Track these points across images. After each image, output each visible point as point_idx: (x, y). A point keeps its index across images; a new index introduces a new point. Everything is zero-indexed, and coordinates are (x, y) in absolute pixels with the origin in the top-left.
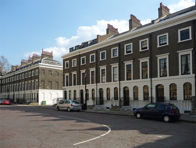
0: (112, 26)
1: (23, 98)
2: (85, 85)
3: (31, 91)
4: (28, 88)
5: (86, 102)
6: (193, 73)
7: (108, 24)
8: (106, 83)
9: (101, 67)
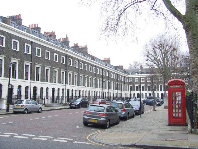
2: (8, 79)
9: (14, 58)
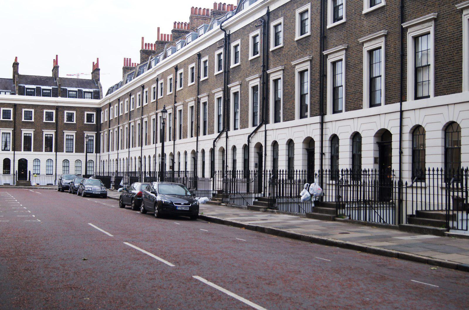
0: (130, 59)
1: (189, 169)
3: (396, 106)
4: (198, 127)
5: (185, 189)
6: (12, 151)
7: (125, 58)
8: (434, 100)
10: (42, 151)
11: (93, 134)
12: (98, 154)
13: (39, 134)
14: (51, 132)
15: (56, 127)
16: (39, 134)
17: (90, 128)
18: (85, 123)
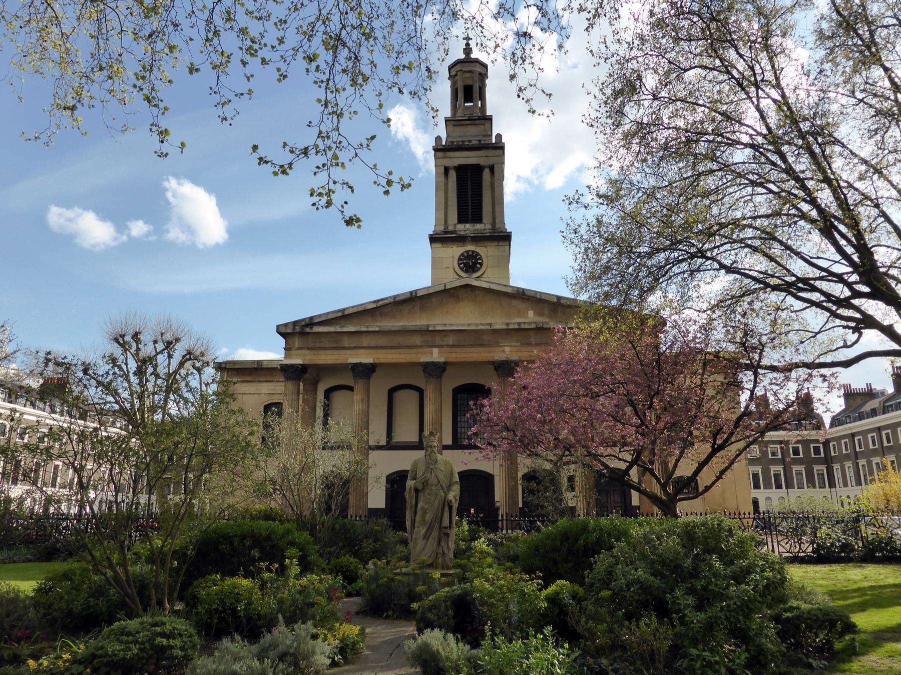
10: (772, 488)
11: (823, 467)
12: (833, 490)
13: (766, 472)
14: (780, 468)
15: (783, 461)
16: (766, 472)
17: (819, 461)
18: (813, 456)
